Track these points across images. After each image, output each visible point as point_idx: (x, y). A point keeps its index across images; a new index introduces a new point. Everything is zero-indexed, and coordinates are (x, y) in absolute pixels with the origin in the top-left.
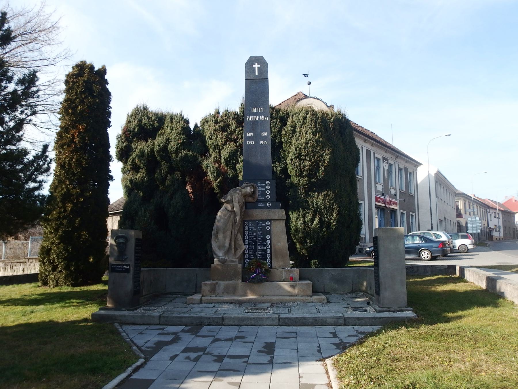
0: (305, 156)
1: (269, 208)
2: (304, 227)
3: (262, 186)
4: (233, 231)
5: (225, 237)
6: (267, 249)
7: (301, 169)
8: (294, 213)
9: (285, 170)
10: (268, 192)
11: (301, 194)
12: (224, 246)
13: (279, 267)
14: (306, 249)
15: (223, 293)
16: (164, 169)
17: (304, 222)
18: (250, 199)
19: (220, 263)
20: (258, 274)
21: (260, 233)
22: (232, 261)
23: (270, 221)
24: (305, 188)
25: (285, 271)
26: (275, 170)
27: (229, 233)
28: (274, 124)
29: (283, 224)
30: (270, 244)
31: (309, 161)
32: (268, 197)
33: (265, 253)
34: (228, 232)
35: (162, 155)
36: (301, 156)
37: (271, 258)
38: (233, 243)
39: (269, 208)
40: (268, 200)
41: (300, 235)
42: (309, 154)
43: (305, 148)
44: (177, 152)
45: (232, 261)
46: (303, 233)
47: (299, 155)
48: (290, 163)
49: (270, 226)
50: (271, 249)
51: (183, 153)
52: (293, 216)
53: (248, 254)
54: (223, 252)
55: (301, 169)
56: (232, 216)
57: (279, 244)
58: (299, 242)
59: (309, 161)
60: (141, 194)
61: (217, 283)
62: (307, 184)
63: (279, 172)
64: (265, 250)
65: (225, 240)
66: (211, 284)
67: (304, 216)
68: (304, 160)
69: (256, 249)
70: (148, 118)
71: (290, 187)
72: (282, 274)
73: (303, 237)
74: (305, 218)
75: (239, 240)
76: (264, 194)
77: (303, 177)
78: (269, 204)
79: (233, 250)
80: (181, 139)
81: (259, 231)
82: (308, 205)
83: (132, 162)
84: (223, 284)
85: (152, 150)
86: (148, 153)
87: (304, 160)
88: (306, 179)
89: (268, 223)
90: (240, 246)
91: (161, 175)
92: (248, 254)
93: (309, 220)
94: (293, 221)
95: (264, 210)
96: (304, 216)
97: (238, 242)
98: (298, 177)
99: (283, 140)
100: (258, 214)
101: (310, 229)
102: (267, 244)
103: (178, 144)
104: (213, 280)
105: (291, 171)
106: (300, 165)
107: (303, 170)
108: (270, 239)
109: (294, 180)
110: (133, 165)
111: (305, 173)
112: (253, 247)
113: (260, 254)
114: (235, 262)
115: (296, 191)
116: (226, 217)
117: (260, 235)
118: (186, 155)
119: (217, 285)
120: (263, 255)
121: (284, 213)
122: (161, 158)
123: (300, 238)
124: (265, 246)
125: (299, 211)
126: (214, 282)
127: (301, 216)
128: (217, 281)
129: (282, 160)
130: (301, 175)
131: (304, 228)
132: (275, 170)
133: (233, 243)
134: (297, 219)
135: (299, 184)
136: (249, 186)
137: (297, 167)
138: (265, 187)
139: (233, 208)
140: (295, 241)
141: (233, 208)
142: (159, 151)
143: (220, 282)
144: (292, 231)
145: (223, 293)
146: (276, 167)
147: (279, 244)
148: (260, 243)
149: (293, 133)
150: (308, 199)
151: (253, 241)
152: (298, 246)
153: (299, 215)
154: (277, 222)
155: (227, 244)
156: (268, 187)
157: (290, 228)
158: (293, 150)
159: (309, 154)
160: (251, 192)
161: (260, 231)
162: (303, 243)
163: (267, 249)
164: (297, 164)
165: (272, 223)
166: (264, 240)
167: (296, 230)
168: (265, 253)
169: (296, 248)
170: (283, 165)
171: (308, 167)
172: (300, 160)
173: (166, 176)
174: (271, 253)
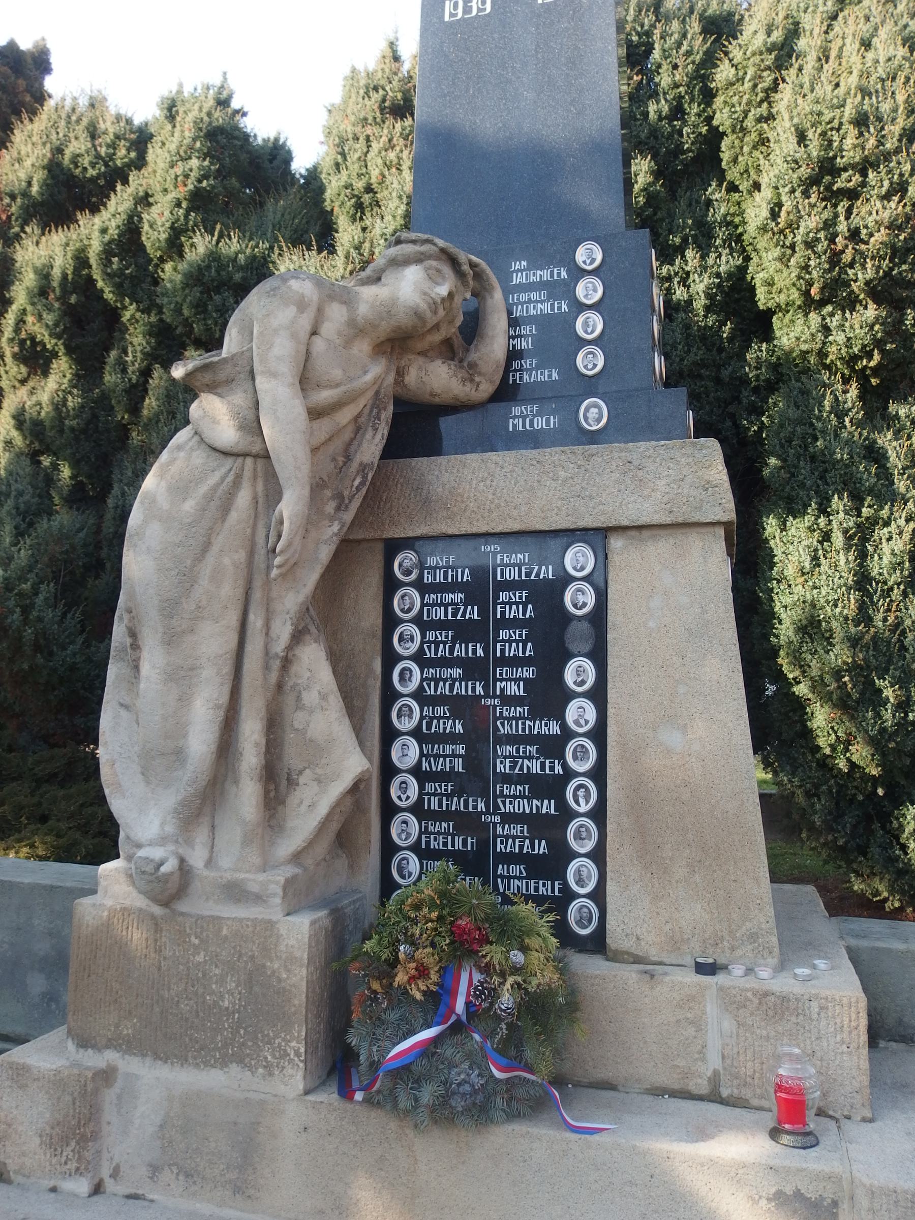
0: (863, 168)
1: (593, 438)
2: (862, 607)
3: (541, 285)
4: (256, 620)
5: (181, 677)
6: (569, 774)
7: (835, 258)
8: (798, 527)
9: (735, 294)
10: (591, 325)
11: (840, 413)
12: (179, 755)
13: (675, 943)
14: (877, 743)
15: (155, 1170)
16: (137, 341)
17: (863, 581)
18: (438, 379)
19: (139, 902)
20: (457, 1028)
21: (512, 643)
22: (235, 892)
23: (598, 536)
24: (863, 377)
25: (732, 1003)
26: (680, 294)
27: (213, 641)
28: (670, 42)
29: (714, 565)
30: (599, 734)
31: (887, 197)
32: (590, 362)
33: (548, 807)
34: (207, 629)
35: (120, 273)
36: (836, 172)
37: (598, 855)
38: (251, 731)
39: (593, 438)
40: (590, 386)
41: (840, 655)
42: (887, 156)
43: (861, 121)
44: (174, 246)
45: (235, 892)
46: (854, 642)
47: (827, 167)
48: (764, 229)
49: (600, 584)
50: (599, 774)
51: (200, 246)
52: (790, 542)
53: (417, 809)
54: (170, 799)
55: (835, 258)
56: (243, 498)
57: (673, 738)
58: (826, 698)
59: (887, 197)
60: (66, 472)
61: (106, 1076)
62: (879, 344)
63: (700, 304)
64: (552, 787)
65: (184, 700)
66: (58, 1082)
67: (861, 539)
68: (852, 195)
69: (476, 777)
70: (93, 133)
71: (771, 387)
72: (698, 1024)
73: (853, 668)
74: (863, 555)
75: (310, 698)
76: (560, 340)
77: (851, 303)
78: (594, 413)
79: (247, 795)
80: (187, 176)
81: (504, 623)
82: (885, 474)
83: (17, 330)
84: (152, 1085)
85: (81, 260)
86: (65, 276)
87: (852, 195)
88: (871, 312)
89: (578, 558)
90: (317, 751)
91: (124, 371)
92: (417, 809)
93: (896, 566)
94: (790, 571)
95: (552, 455)
96: (861, 539)
97: (298, 719)
98: (822, 303)
99: (722, 118)
100: (490, 490)
101: (898, 624)
102: (567, 734)
103: (178, 205)
104: (84, 1043)
105: (774, 277)
106: (829, 225)
107: (847, 257)
108: (598, 695)
109: (793, 334)
110: (22, 342)
111: (861, 276)
112: (454, 759)
113: (508, 819)
114: (259, 899)
115: (805, 399)
116: (189, 506)
117: (515, 662)
118: (213, 257)
119: (109, 1096)
120: (537, 825)
121: (719, 473)
122: (119, 290)
123: (837, 674)
124: (553, 747)
125: (824, 510)
126: (95, 1060)
127: (838, 539)
128: (111, 1056)
129: (721, 234)
130: (835, 294)
131: (864, 616)
132: (680, 294)
133: (251, 731)
134: (815, 560)
135: (822, 354)
136: (418, 259)
137: (810, 245)
138: (566, 290)
139: (252, 426)
140: (802, 690)
141: (252, 426)
142: (107, 254)
143: (131, 1066)
144: (786, 630)
145: (155, 1170)
146: (684, 281)
147: (673, 738)
148: (512, 721)
149: (780, 65)
150: (885, 440)
151: (460, 706)
152: (821, 717)
153: (826, 537)
154: (659, 549)
155: (200, 741)
156: (589, 290)
157: (770, 616)
158: (783, 141)
159: (887, 156)
160: (434, 306)
161: (514, 623)
162: (856, 701)
163: (569, 774)
164: (810, 222)
165: (615, 560)
166: (549, 697)
167: (812, 628)
168: (548, 807)
169: (807, 734)
170: (726, 263)
171: (881, 236)
172: (832, 196)
173: (146, 373)
174: (599, 814)
